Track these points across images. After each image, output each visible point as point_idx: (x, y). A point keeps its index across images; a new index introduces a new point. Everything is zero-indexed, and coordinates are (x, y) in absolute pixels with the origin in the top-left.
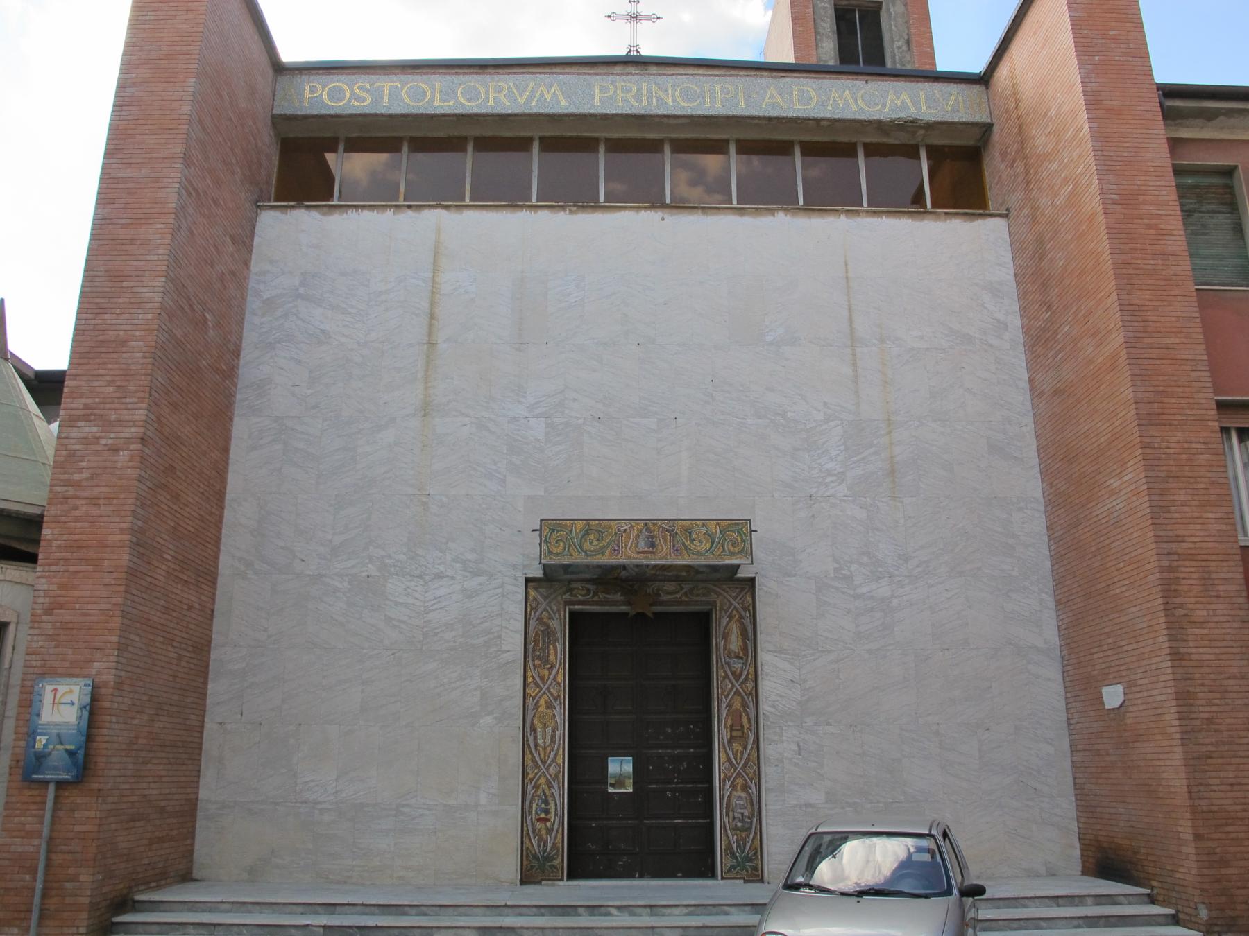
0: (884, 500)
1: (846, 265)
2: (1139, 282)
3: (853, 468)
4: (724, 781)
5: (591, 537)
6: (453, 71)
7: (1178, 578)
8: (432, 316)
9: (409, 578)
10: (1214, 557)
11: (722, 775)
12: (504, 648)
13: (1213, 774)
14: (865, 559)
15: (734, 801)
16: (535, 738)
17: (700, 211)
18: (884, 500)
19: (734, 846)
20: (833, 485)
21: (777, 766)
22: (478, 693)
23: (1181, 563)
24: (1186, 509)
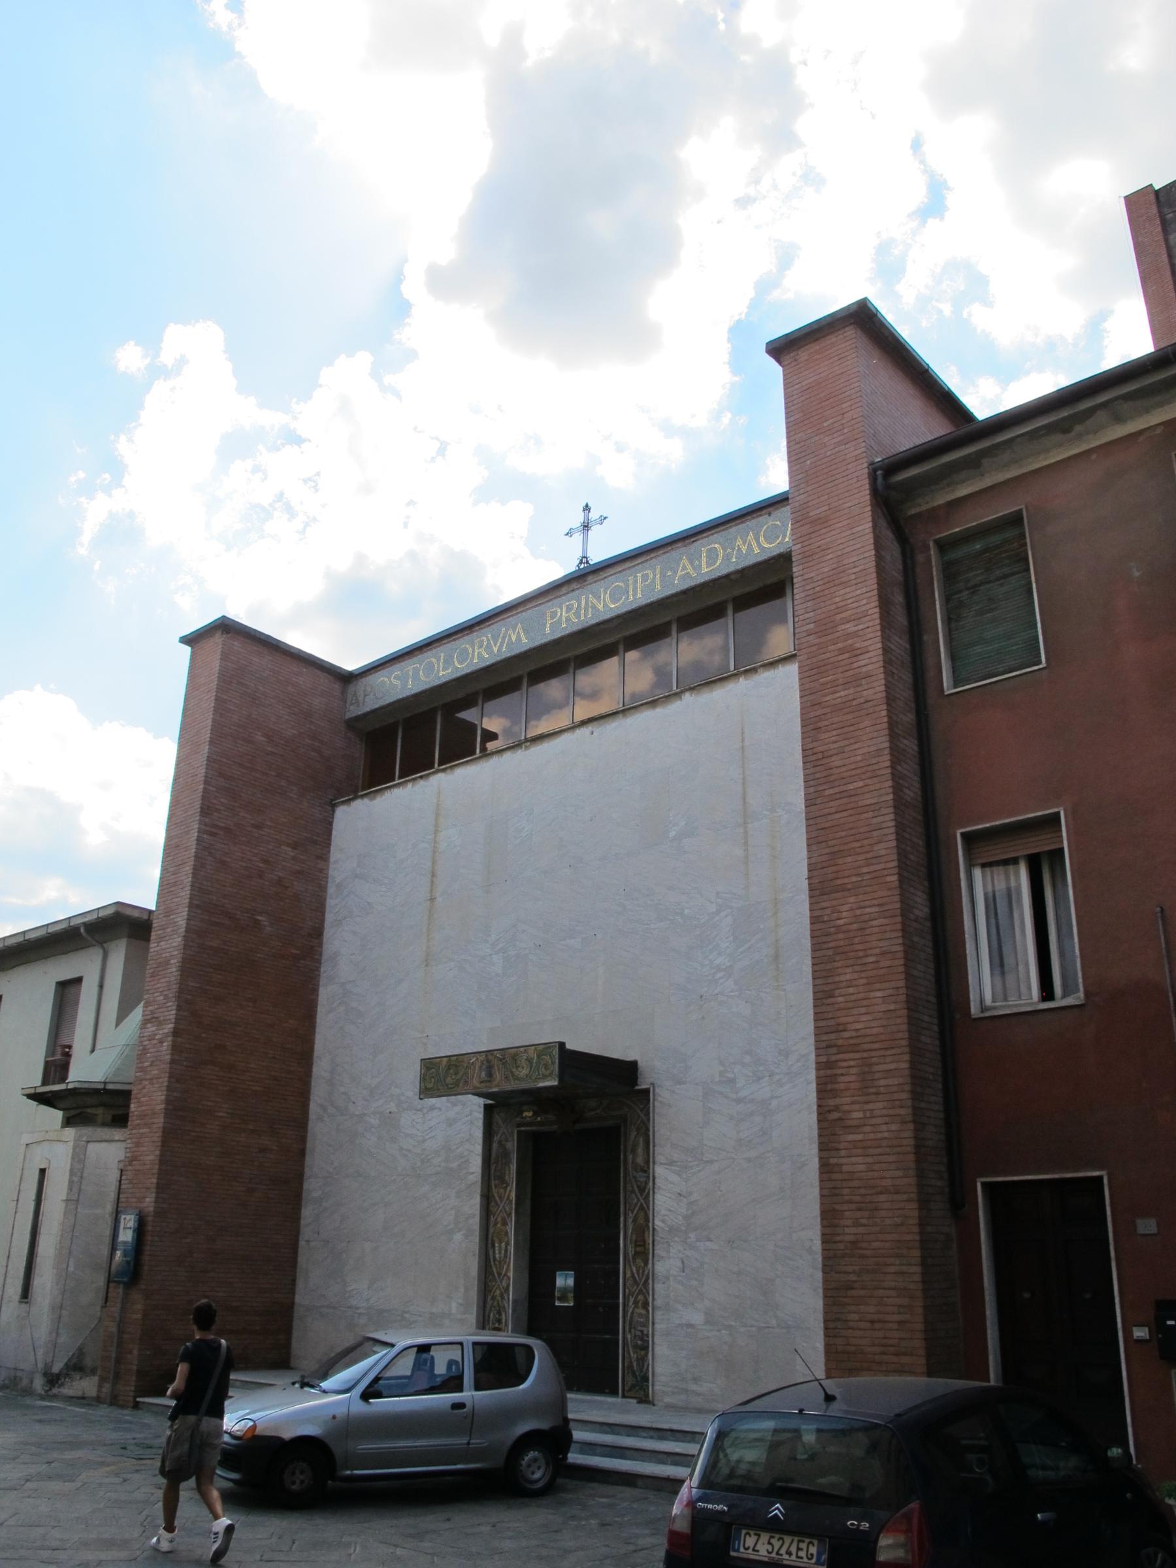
0: (768, 990)
1: (743, 733)
2: (826, 723)
3: (740, 960)
4: (629, 1298)
5: (451, 1071)
6: (451, 639)
7: (836, 1075)
8: (433, 875)
9: (414, 1111)
10: (876, 1046)
11: (627, 1291)
12: (471, 1171)
13: (853, 1308)
14: (747, 1059)
15: (636, 1318)
16: (494, 1252)
17: (621, 715)
18: (768, 990)
19: (635, 1364)
20: (722, 981)
21: (664, 1283)
22: (453, 1212)
23: (841, 1056)
24: (851, 990)
